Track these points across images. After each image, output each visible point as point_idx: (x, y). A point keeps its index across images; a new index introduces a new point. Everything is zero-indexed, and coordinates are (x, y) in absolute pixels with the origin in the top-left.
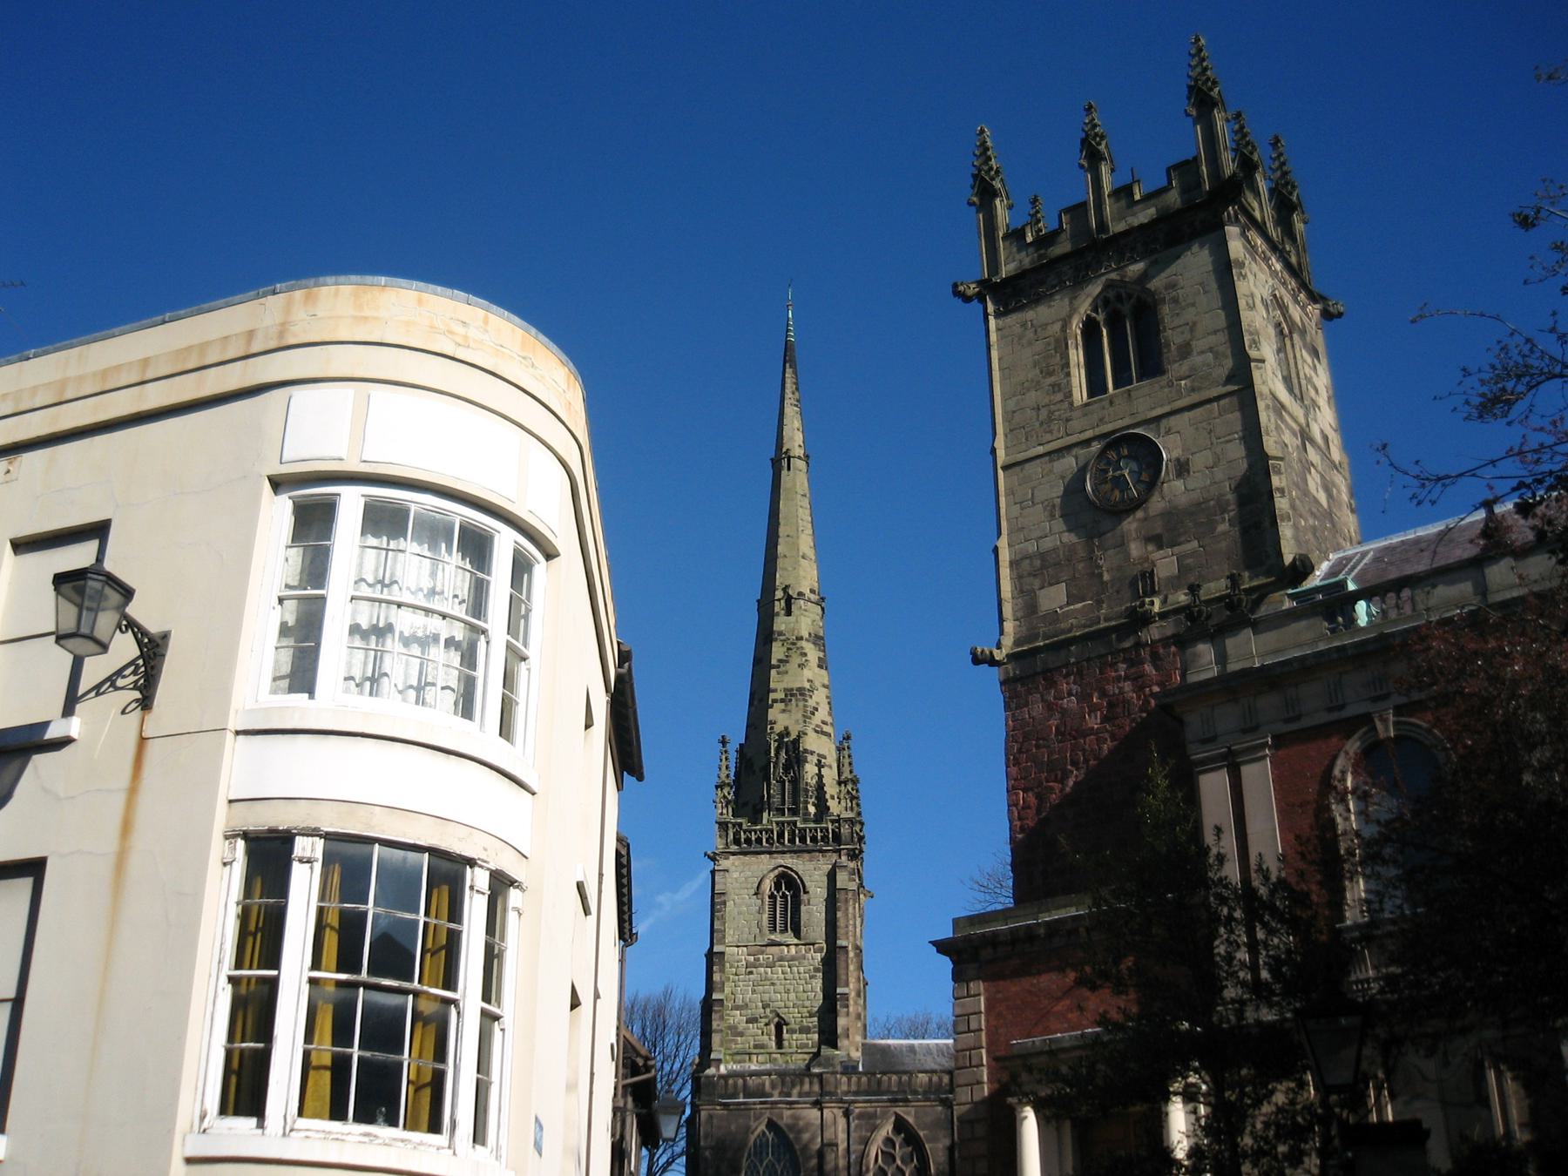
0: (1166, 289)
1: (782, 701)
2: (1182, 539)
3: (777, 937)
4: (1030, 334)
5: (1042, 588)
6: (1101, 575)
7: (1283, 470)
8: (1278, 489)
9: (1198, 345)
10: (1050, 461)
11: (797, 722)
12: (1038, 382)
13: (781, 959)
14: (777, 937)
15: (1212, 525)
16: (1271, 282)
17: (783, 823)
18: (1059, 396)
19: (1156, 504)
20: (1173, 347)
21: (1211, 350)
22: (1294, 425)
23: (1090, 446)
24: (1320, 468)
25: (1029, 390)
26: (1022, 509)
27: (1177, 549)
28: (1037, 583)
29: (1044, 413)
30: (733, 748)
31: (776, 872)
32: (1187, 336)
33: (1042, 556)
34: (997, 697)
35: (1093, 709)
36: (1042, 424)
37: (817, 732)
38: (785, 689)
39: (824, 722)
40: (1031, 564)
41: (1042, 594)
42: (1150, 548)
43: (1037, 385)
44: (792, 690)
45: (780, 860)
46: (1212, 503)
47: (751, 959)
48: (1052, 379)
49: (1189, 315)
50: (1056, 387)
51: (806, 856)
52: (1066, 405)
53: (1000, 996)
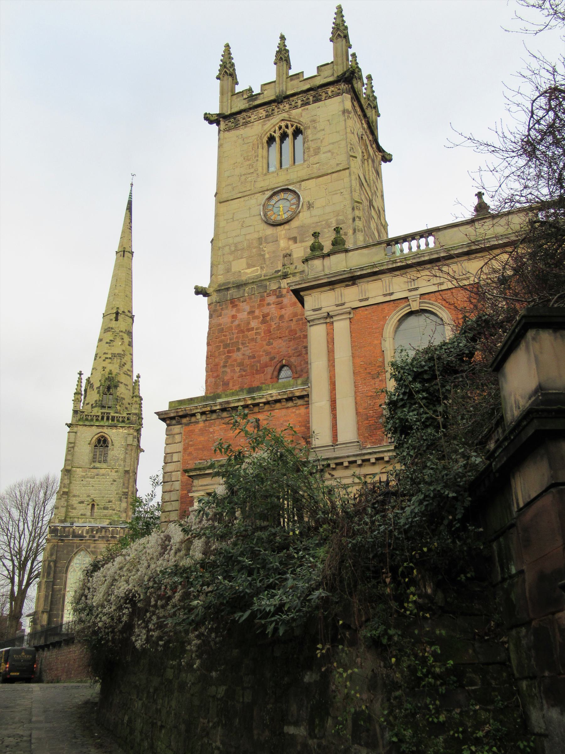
0: (311, 122)
1: (110, 358)
2: (307, 239)
3: (98, 465)
4: (240, 141)
5: (234, 260)
6: (264, 255)
7: (361, 209)
8: (358, 217)
9: (323, 149)
11: (116, 368)
13: (97, 475)
16: (362, 130)
19: (294, 224)
20: (311, 149)
21: (329, 151)
22: (368, 198)
24: (376, 220)
26: (227, 223)
27: (304, 244)
28: (231, 258)
29: (243, 178)
30: (84, 378)
31: (99, 435)
33: (236, 245)
34: (206, 313)
35: (255, 318)
37: (125, 374)
38: (112, 354)
39: (128, 370)
40: (230, 249)
41: (234, 263)
44: (115, 354)
45: (101, 430)
46: (324, 223)
47: (84, 474)
49: (320, 135)
50: (251, 166)
52: (255, 175)
53: (191, 443)
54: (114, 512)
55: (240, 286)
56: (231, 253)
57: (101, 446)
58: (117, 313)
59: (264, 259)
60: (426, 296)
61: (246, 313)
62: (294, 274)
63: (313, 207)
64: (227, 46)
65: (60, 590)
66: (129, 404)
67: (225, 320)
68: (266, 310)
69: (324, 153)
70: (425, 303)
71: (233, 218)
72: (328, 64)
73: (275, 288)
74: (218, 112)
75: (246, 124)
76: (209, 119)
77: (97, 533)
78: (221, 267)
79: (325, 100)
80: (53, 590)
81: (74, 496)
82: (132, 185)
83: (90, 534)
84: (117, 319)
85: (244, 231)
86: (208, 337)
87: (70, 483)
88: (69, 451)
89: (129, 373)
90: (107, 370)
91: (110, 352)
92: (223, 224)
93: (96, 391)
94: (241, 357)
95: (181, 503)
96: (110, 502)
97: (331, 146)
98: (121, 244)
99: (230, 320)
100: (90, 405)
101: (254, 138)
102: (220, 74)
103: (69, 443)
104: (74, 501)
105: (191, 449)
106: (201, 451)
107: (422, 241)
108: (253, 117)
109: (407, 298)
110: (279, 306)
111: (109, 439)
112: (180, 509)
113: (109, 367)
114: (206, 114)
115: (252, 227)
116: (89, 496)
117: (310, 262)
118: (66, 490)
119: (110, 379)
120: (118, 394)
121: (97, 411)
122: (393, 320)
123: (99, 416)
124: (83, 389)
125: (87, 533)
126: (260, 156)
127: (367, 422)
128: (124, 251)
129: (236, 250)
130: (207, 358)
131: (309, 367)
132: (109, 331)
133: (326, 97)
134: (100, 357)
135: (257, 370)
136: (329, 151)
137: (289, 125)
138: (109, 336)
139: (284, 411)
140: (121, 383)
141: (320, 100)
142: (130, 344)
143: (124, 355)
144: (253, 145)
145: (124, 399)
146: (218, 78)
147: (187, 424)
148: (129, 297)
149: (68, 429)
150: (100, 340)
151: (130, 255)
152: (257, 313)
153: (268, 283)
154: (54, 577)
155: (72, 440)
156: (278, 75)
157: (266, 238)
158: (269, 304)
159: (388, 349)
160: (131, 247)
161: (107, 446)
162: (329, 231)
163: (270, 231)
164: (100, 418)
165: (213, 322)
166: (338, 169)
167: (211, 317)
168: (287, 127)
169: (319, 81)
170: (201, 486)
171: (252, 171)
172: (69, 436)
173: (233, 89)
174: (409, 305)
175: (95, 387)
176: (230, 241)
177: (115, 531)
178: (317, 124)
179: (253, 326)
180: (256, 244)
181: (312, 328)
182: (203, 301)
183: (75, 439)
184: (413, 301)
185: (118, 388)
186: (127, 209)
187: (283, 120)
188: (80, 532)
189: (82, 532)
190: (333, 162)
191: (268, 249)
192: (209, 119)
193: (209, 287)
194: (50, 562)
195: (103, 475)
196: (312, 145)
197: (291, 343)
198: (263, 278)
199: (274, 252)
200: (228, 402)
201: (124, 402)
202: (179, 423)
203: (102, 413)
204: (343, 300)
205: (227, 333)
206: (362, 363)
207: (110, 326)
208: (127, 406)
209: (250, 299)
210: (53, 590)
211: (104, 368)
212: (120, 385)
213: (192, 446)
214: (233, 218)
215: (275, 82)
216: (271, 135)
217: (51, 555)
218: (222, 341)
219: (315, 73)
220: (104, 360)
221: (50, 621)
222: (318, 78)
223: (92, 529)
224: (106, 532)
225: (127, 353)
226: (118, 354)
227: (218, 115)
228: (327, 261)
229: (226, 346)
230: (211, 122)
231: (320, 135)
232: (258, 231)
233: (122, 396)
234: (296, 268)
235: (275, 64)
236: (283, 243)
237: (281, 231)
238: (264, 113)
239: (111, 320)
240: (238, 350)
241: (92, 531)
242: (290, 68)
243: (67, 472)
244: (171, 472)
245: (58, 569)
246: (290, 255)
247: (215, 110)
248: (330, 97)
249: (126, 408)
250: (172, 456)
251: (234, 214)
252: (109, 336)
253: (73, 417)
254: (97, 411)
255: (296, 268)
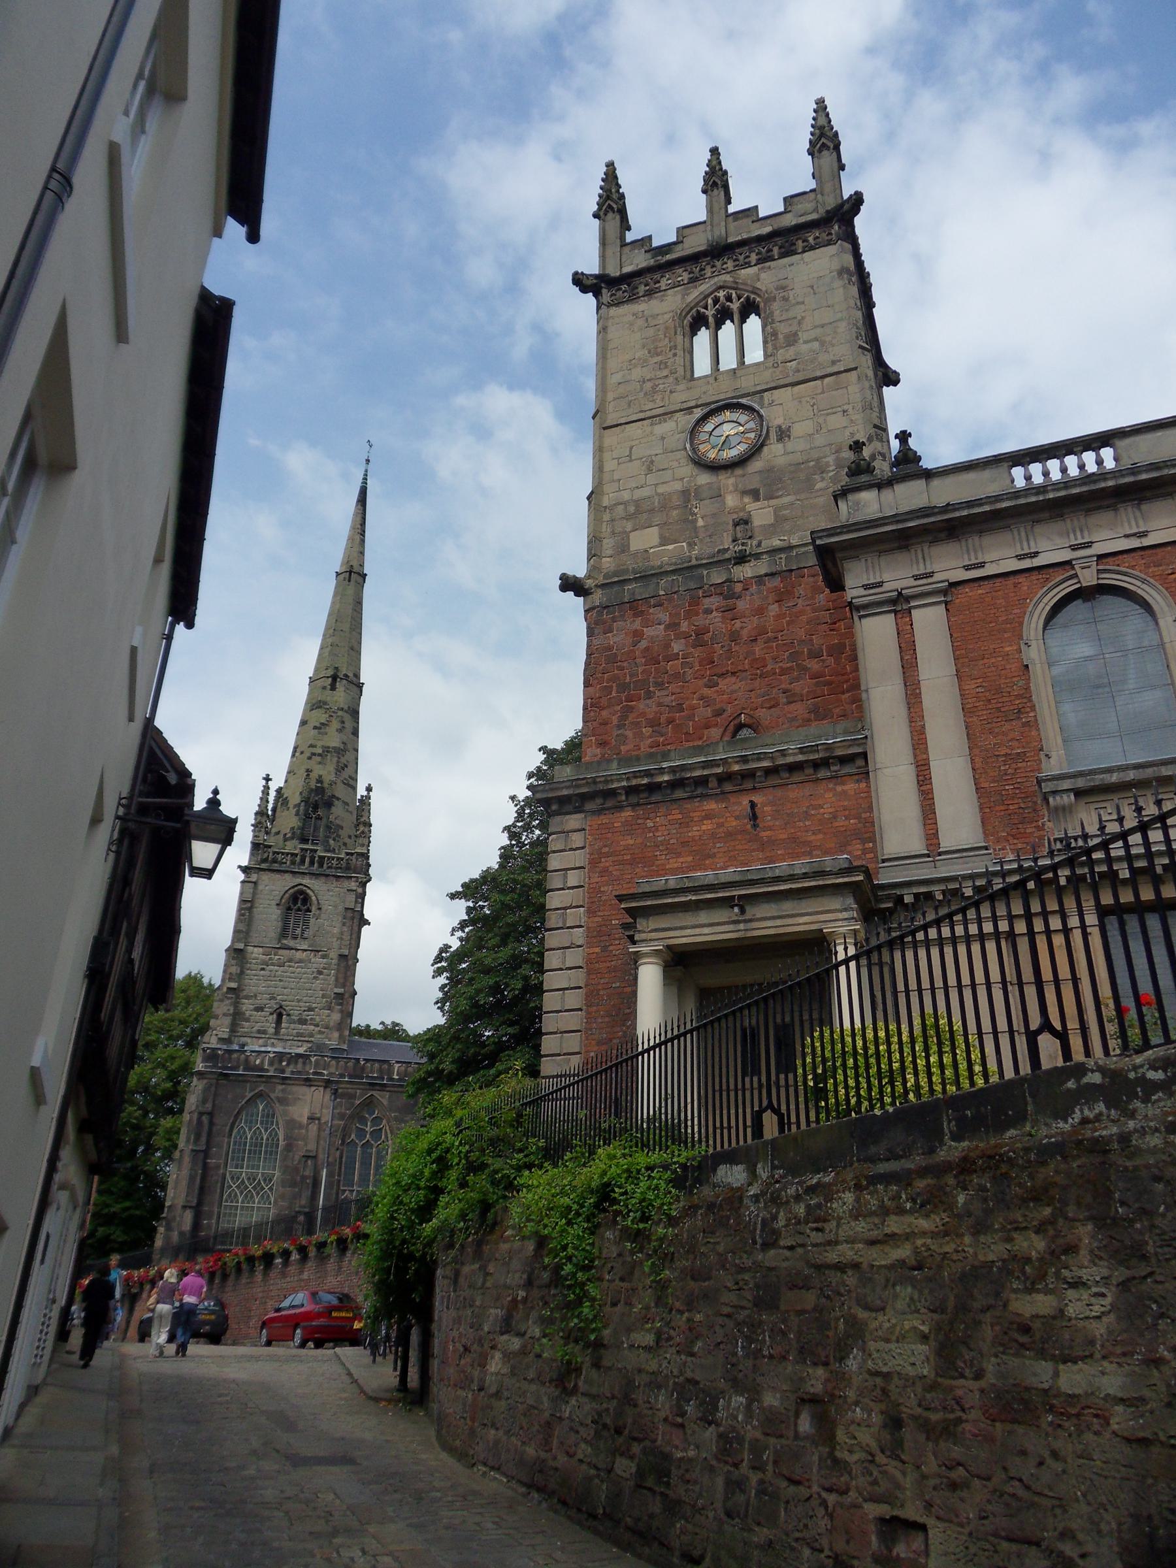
0: (777, 289)
1: (320, 755)
6: (696, 520)
8: (880, 453)
9: (803, 336)
10: (652, 425)
11: (329, 773)
12: (645, 361)
13: (290, 961)
14: (291, 943)
15: (809, 484)
17: (306, 850)
18: (665, 372)
19: (756, 465)
20: (781, 336)
21: (816, 339)
23: (691, 413)
25: (635, 366)
27: (773, 502)
28: (629, 526)
29: (648, 385)
30: (274, 786)
32: (794, 328)
33: (637, 503)
35: (677, 637)
36: (646, 394)
42: (746, 500)
43: (644, 363)
45: (298, 880)
46: (812, 464)
48: (660, 358)
49: (797, 312)
50: (662, 365)
51: (323, 879)
52: (671, 379)
53: (606, 850)
54: (317, 1029)
55: (644, 577)
56: (628, 517)
57: (299, 910)
58: (334, 678)
59: (695, 528)
60: (1110, 560)
61: (662, 627)
62: (757, 556)
63: (789, 437)
64: (611, 165)
65: (218, 1167)
66: (350, 837)
67: (618, 638)
68: (701, 621)
69: (806, 342)
70: (1109, 571)
71: (630, 456)
72: (804, 193)
73: (719, 581)
74: (597, 272)
75: (650, 294)
76: (579, 281)
77: (288, 1065)
78: (608, 544)
79: (804, 252)
80: (205, 1167)
81: (247, 997)
82: (368, 461)
83: (276, 1066)
84: (333, 688)
85: (651, 479)
86: (585, 670)
87: (242, 972)
88: (243, 915)
89: (351, 782)
90: (314, 775)
91: (319, 744)
92: (610, 465)
93: (294, 811)
94: (654, 708)
95: (589, 973)
96: (310, 1009)
97: (819, 330)
98: (347, 561)
99: (629, 640)
100: (281, 836)
101: (667, 316)
102: (600, 209)
103: (242, 901)
104: (247, 1006)
105: (605, 863)
106: (628, 867)
107: (1089, 457)
108: (663, 284)
109: (1068, 564)
110: (729, 615)
111: (314, 898)
112: (586, 985)
113: (318, 771)
114: (576, 274)
115: (669, 472)
116: (274, 998)
117: (850, 497)
118: (233, 985)
119: (320, 790)
120: (332, 818)
121: (294, 846)
122: (1041, 605)
123: (296, 855)
124: (270, 806)
125: (271, 1063)
126: (680, 347)
127: (1003, 808)
128: (350, 572)
129: (640, 513)
130: (585, 708)
131: (864, 696)
132: (320, 707)
133: (804, 247)
134: (302, 753)
135: (687, 733)
136: (816, 339)
137: (734, 295)
138: (320, 716)
139: (808, 789)
140: (338, 799)
141: (794, 253)
142: (355, 733)
143: (345, 750)
144: (667, 328)
145: (342, 828)
146: (596, 216)
147: (599, 812)
148: (355, 650)
149: (242, 876)
150: (303, 723)
151: (360, 579)
152: (684, 626)
153: (705, 572)
154: (208, 1143)
155: (249, 897)
156: (710, 210)
157: (698, 490)
158: (708, 611)
159: (1037, 662)
160: (362, 566)
161: (309, 910)
162: (823, 479)
163: (704, 478)
164: (298, 859)
165: (596, 642)
166: (835, 369)
167: (590, 633)
168: (729, 298)
169: (790, 220)
170: (656, 930)
171: (665, 372)
172: (242, 888)
173: (622, 237)
174: (1076, 576)
175: (291, 805)
176: (626, 496)
177: (322, 1063)
178: (791, 293)
179: (675, 651)
180: (676, 501)
181: (864, 621)
182: (575, 604)
183: (254, 894)
184: (1083, 568)
185: (333, 809)
186: (358, 501)
187: (721, 287)
188: (258, 1062)
189: (262, 1062)
190: (824, 358)
191: (702, 514)
192: (579, 281)
193: (588, 576)
194: (201, 1114)
195: (300, 961)
196: (783, 329)
197: (757, 683)
198: (694, 562)
199: (714, 515)
200: (683, 768)
201: (341, 832)
202: (578, 810)
203: (302, 849)
204: (928, 566)
205: (625, 664)
206: (979, 690)
207: (322, 698)
208: (347, 840)
209: (670, 600)
210: (205, 1167)
211: (308, 770)
212: (336, 802)
213: (607, 855)
214: (630, 456)
215: (704, 222)
216: (698, 311)
217: (204, 1101)
218: (614, 679)
219: (780, 208)
220: (310, 758)
221: (196, 1225)
222: (789, 216)
223: (280, 1056)
224: (304, 1063)
225: (349, 746)
226: (334, 748)
227: (596, 277)
228: (887, 495)
229: (623, 687)
230: (584, 289)
231: (797, 312)
232: (682, 479)
233: (337, 822)
234: (759, 545)
235: (704, 191)
236: (731, 501)
237: (727, 481)
238: (686, 276)
239: (324, 688)
240: (649, 695)
241: (281, 1061)
242: (730, 203)
243: (236, 954)
244: (565, 908)
245: (215, 1129)
246: (746, 522)
247: (591, 266)
248: (812, 248)
249: (345, 844)
250: (565, 877)
251: (631, 448)
252: (320, 716)
253: (252, 854)
254: (294, 846)
255: (759, 545)
